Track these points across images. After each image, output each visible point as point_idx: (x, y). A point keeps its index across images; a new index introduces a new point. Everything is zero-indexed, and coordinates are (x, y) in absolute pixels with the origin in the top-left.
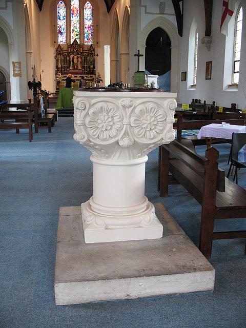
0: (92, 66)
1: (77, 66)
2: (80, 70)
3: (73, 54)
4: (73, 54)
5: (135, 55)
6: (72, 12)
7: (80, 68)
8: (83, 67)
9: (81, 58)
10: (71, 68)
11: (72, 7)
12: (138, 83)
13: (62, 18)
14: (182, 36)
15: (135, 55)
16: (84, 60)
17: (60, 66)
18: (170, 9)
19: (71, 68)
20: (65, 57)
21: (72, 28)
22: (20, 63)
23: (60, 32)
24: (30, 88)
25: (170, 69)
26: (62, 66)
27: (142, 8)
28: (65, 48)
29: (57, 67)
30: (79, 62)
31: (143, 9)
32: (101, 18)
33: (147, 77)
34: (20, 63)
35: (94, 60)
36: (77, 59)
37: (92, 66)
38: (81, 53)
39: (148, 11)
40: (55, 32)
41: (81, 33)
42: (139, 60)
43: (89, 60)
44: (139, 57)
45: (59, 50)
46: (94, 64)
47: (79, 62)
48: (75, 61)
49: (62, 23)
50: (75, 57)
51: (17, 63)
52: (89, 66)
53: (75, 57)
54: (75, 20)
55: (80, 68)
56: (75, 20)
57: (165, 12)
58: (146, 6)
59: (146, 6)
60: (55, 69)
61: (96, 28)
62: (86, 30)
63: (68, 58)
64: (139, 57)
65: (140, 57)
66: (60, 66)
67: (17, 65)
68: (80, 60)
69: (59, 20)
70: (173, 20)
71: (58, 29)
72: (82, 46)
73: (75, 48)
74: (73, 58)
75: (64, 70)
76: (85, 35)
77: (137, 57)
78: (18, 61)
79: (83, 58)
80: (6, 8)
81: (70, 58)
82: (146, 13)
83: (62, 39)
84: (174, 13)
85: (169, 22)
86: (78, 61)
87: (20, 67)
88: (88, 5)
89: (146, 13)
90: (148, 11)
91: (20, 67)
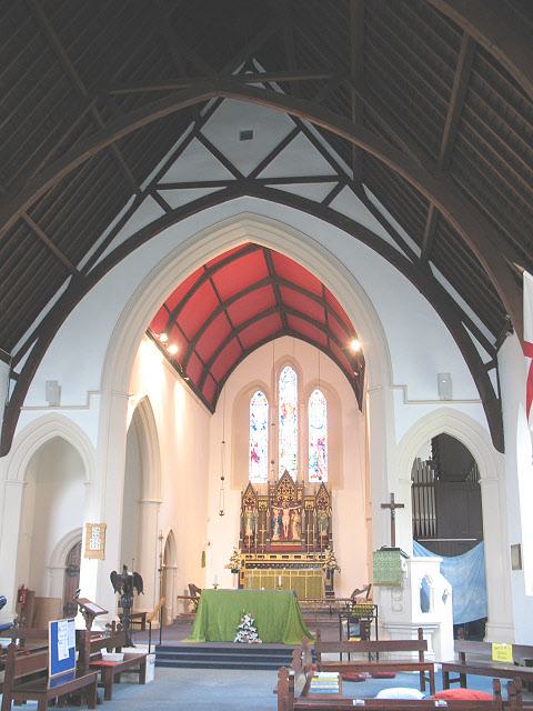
0: (323, 533)
1: (290, 532)
2: (295, 541)
3: (279, 504)
4: (279, 504)
5: (384, 506)
6: (281, 413)
7: (295, 536)
8: (304, 535)
9: (300, 514)
10: (276, 537)
11: (281, 403)
12: (382, 579)
13: (259, 426)
14: (213, 411)
15: (384, 506)
16: (307, 517)
17: (249, 532)
18: (466, 387)
19: (276, 537)
20: (262, 512)
21: (280, 447)
22: (103, 527)
23: (255, 456)
24: (117, 589)
25: (481, 539)
26: (254, 533)
27: (395, 391)
28: (264, 492)
29: (243, 534)
30: (294, 523)
31: (398, 393)
32: (345, 421)
33: (409, 563)
34: (103, 527)
35: (329, 519)
36: (290, 515)
37: (323, 533)
38: (300, 502)
39: (410, 396)
40: (244, 455)
41: (302, 456)
42: (393, 519)
43: (318, 519)
44: (392, 509)
45: (249, 498)
46: (329, 529)
47: (294, 523)
48: (286, 521)
49: (259, 438)
50: (286, 511)
51: (96, 525)
52: (318, 532)
53: (286, 511)
54: (288, 429)
55: (295, 536)
56: (288, 429)
57: (454, 398)
58: (404, 387)
59: (404, 387)
60: (239, 539)
61: (335, 447)
62: (312, 451)
63: (268, 515)
64: (392, 509)
65: (397, 510)
66: (249, 532)
67: (96, 531)
68: (296, 518)
69: (252, 430)
70: (477, 413)
71: (251, 449)
72: (298, 487)
73: (284, 489)
74: (281, 513)
75: (259, 542)
76: (311, 462)
77: (389, 510)
78: (98, 522)
79: (304, 514)
80: (87, 407)
81: (272, 514)
82: (406, 401)
83: (259, 475)
84: (479, 397)
85: (469, 423)
86: (291, 521)
87: (103, 537)
88: (317, 397)
89: (406, 401)
90: (410, 396)
91: (103, 537)
